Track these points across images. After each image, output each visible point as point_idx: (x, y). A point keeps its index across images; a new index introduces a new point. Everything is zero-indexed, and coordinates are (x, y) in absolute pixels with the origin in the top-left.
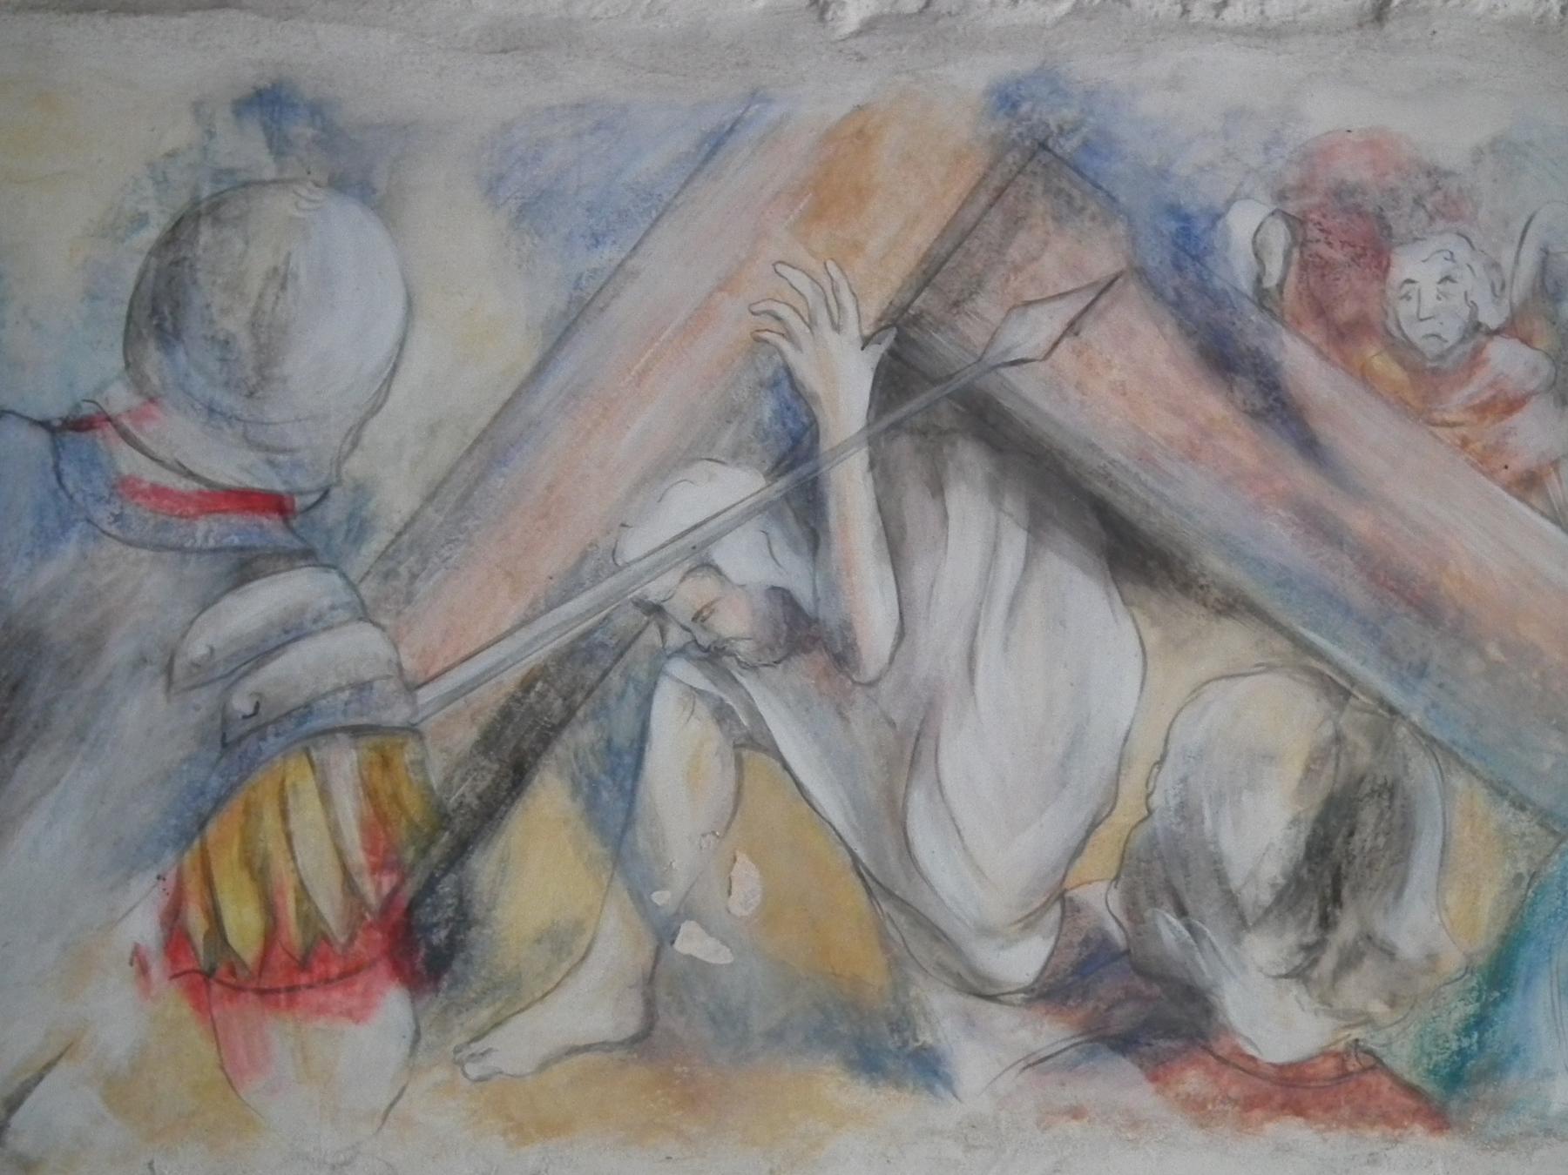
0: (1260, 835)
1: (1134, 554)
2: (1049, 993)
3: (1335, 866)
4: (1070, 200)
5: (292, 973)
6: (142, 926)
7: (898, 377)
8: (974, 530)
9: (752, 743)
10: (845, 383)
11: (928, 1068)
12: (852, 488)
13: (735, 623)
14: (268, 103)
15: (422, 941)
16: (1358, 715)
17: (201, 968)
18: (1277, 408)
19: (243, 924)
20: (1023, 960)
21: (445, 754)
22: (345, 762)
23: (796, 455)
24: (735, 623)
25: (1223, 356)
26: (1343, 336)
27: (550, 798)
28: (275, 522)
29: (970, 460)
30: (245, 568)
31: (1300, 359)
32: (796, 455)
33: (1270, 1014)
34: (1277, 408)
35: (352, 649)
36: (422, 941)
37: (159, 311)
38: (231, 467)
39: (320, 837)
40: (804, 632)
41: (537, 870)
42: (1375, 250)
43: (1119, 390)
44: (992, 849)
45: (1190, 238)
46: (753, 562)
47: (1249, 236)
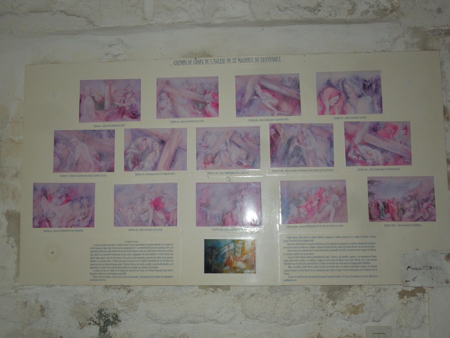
0: (244, 157)
1: (239, 147)
2: (236, 163)
3: (247, 158)
4: (217, 256)
5: (208, 163)
6: (203, 162)
7: (230, 141)
8: (233, 146)
9: (225, 154)
10: (228, 141)
11: (232, 166)
12: (228, 145)
13: (224, 150)
14: (207, 132)
15: (213, 162)
16: (338, 105)
17: (205, 163)
18: (244, 141)
19: (206, 161)
20: (235, 162)
21: (213, 156)
22: (210, 156)
23: (226, 143)
24: (224, 150)
25: (242, 139)
26: (247, 138)
27: (217, 156)
28: (207, 147)
29: (233, 143)
30: (206, 149)
31: (245, 139)
32: (226, 143)
33: (245, 164)
34: (244, 141)
35: (210, 151)
36: (213, 162)
37: (203, 140)
38: (205, 145)
39: (209, 159)
40: (227, 150)
41: (217, 159)
42: (248, 135)
43: (238, 141)
44: (234, 158)
45: (241, 135)
46: (225, 148)
47: (243, 135)
